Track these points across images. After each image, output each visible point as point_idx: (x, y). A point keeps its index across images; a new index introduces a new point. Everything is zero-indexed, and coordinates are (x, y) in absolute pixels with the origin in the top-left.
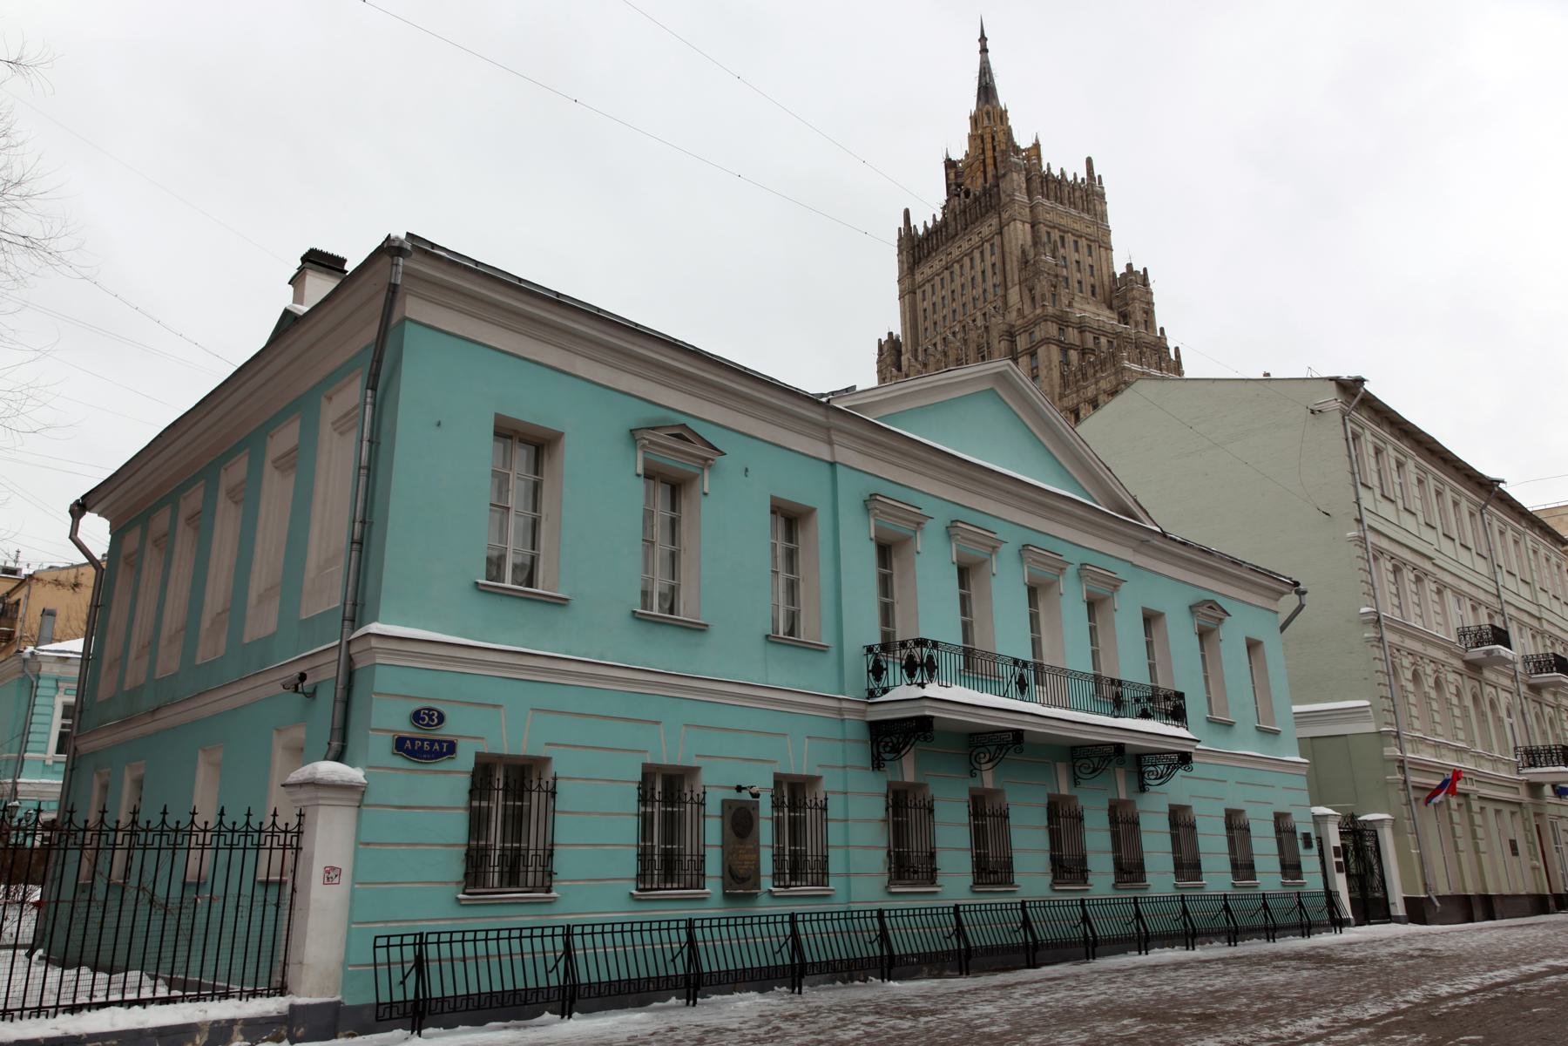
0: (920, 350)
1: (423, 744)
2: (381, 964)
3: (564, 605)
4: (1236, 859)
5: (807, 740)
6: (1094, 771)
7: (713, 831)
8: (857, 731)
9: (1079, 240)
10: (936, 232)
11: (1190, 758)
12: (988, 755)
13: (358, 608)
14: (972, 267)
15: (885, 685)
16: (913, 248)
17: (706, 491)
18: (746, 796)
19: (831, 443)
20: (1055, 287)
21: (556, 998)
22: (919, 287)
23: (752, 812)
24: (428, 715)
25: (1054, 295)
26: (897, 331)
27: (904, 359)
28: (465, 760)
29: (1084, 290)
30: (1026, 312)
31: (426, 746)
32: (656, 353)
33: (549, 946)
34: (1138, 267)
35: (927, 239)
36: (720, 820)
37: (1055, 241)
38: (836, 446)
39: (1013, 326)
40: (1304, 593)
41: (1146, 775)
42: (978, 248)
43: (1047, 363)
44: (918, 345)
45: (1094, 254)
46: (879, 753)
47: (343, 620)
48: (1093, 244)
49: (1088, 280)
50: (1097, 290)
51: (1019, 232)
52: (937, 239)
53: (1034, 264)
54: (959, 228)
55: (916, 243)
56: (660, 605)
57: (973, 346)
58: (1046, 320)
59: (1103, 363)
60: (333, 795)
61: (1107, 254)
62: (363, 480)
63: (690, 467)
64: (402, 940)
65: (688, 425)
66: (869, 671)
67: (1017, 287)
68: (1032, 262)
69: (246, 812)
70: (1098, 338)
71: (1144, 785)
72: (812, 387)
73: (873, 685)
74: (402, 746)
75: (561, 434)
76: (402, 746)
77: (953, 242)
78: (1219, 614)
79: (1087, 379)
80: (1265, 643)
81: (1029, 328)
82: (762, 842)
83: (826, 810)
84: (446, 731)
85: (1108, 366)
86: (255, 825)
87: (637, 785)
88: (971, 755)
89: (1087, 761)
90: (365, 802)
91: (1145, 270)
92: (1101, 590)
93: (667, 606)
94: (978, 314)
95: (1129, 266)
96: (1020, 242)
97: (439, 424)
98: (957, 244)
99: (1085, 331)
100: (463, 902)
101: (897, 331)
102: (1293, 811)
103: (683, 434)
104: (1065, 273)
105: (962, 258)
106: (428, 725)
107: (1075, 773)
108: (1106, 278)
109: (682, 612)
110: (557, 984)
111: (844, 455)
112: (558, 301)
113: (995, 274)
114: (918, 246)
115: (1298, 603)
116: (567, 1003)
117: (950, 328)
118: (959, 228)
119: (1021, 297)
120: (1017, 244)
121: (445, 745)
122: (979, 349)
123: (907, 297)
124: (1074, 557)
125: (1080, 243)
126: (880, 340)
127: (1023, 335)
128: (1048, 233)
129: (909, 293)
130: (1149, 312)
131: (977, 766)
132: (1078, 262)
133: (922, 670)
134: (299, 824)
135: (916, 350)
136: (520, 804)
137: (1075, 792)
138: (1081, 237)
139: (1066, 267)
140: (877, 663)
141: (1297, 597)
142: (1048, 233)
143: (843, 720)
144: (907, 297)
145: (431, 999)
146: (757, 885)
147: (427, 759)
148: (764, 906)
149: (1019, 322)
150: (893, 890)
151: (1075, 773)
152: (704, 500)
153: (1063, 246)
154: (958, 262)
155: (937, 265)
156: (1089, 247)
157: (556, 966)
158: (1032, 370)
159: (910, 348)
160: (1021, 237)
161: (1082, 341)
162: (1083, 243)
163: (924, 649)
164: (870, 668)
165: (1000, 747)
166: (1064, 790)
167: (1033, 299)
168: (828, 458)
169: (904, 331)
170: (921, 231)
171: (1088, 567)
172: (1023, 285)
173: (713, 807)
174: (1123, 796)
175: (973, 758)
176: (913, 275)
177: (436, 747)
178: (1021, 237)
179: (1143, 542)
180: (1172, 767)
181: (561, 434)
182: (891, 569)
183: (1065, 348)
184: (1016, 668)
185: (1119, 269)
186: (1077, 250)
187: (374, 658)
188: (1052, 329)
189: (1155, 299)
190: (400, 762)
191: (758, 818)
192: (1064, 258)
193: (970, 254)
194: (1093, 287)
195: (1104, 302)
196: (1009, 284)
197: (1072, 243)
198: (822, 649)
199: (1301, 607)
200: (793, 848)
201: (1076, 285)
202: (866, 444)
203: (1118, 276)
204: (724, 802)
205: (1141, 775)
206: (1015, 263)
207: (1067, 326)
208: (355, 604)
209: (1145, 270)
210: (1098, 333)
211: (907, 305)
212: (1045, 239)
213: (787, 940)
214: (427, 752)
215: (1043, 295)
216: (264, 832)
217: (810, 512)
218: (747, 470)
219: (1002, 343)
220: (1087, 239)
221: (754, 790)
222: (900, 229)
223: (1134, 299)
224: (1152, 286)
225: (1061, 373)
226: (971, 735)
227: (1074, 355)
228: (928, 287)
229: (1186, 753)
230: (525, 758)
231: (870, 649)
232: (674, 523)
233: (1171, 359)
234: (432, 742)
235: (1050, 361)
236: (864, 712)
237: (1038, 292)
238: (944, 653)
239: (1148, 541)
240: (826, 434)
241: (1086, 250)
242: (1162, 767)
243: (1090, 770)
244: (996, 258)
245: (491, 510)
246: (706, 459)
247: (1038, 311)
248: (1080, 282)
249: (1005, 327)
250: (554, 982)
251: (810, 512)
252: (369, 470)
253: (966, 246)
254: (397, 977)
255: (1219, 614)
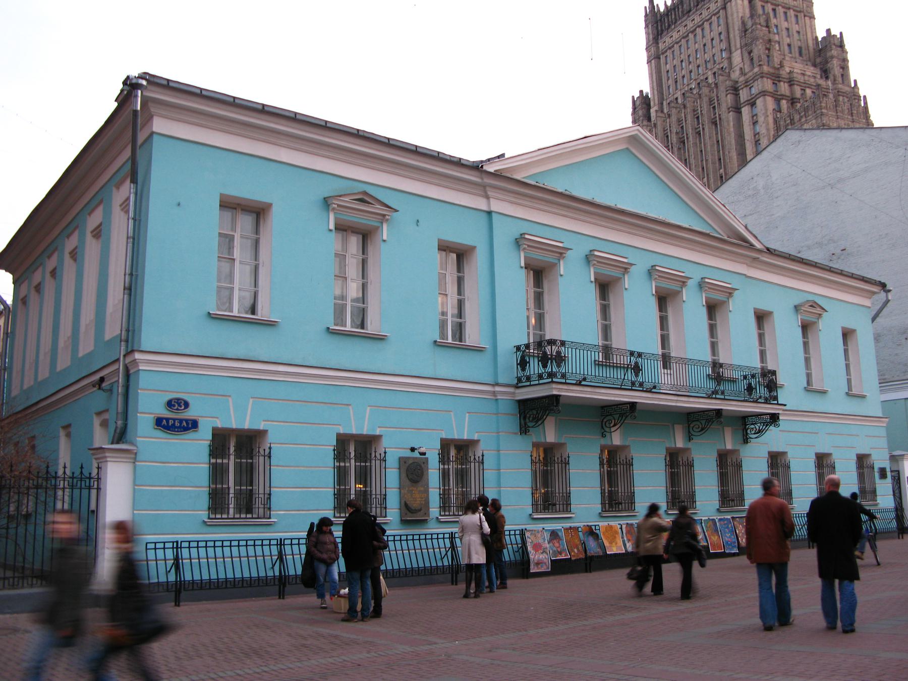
0: (665, 103)
1: (174, 422)
2: (194, 559)
3: (482, 351)
4: (865, 488)
5: (467, 414)
6: (702, 429)
7: (393, 477)
8: (507, 407)
9: (788, 11)
10: (674, 9)
11: (778, 418)
12: (613, 421)
13: (130, 333)
14: (703, 37)
15: (528, 374)
16: (657, 22)
17: (385, 237)
18: (416, 454)
19: (488, 198)
20: (769, 50)
21: (448, 572)
22: (663, 54)
23: (423, 466)
24: (177, 403)
25: (768, 56)
26: (647, 89)
27: (653, 111)
28: (204, 435)
29: (793, 51)
30: (747, 71)
31: (177, 424)
32: (345, 141)
33: (267, 552)
34: (835, 32)
35: (667, 15)
36: (398, 470)
37: (768, 13)
38: (491, 199)
39: (737, 82)
40: (890, 291)
41: (749, 431)
42: (707, 20)
43: (763, 112)
44: (663, 99)
45: (800, 22)
46: (525, 424)
47: (121, 342)
48: (799, 14)
49: (796, 44)
50: (804, 51)
51: (739, 7)
52: (675, 15)
53: (752, 32)
54: (692, 5)
55: (659, 18)
56: (352, 321)
57: (705, 100)
58: (762, 77)
59: (806, 110)
60: (122, 455)
61: (811, 22)
62: (130, 245)
63: (372, 222)
64: (231, 543)
65: (367, 191)
66: (517, 364)
67: (739, 51)
68: (750, 30)
69: (63, 466)
70: (804, 90)
71: (747, 439)
72: (472, 155)
73: (521, 374)
74: (160, 423)
75: (270, 205)
76: (160, 423)
77: (689, 16)
78: (818, 311)
79: (794, 123)
80: (858, 332)
81: (748, 84)
82: (431, 485)
83: (483, 463)
84: (190, 414)
85: (810, 113)
86: (86, 474)
87: (333, 448)
88: (602, 422)
89: (699, 423)
90: (138, 459)
91: (841, 34)
92: (717, 296)
93: (359, 323)
94: (710, 73)
95: (828, 31)
96: (740, 15)
97: (179, 205)
98: (691, 18)
99: (794, 84)
100: (208, 524)
101: (647, 89)
102: (872, 452)
103: (364, 199)
104: (777, 38)
105: (695, 30)
106: (177, 409)
107: (689, 432)
108: (810, 43)
109: (369, 328)
110: (448, 564)
111: (496, 206)
112: (264, 110)
113: (721, 41)
114: (661, 20)
115: (885, 299)
116: (454, 575)
117: (688, 85)
118: (692, 5)
119: (742, 59)
120: (738, 17)
121: (190, 422)
122: (711, 102)
123: (653, 61)
124: (695, 275)
125: (788, 14)
126: (633, 97)
127: (744, 89)
128: (763, 7)
129: (654, 58)
130: (844, 66)
131: (607, 430)
132: (788, 29)
133: (552, 362)
134: (98, 473)
135: (662, 104)
136: (251, 461)
137: (689, 445)
138: (789, 9)
139: (778, 33)
140: (523, 358)
141: (885, 294)
142: (763, 7)
143: (497, 400)
144: (653, 61)
145: (289, 575)
146: (427, 513)
147: (178, 431)
148: (433, 528)
149: (741, 79)
150: (535, 517)
151: (689, 432)
152: (383, 245)
153: (775, 16)
154: (692, 32)
155: (675, 36)
156: (796, 16)
157: (446, 554)
158: (753, 117)
159: (657, 102)
160: (741, 10)
161: (792, 92)
162: (791, 13)
163: (553, 347)
164: (518, 362)
165: (621, 415)
166: (680, 444)
167: (752, 59)
168: (485, 208)
169: (652, 88)
170: (662, 9)
171: (707, 280)
172: (744, 49)
173: (392, 462)
174: (729, 446)
175: (604, 423)
176: (658, 43)
177: (184, 424)
178: (741, 10)
179: (755, 259)
180: (767, 424)
181: (270, 205)
182: (542, 288)
183: (778, 99)
184: (632, 358)
185: (821, 34)
186: (786, 20)
187: (138, 366)
188: (768, 85)
189: (849, 57)
190: (159, 433)
191: (428, 469)
192: (777, 26)
193: (701, 26)
194: (800, 48)
195: (810, 60)
196: (733, 49)
197: (782, 14)
198: (479, 350)
199: (888, 301)
200: (609, 469)
201: (786, 47)
202: (516, 196)
203: (820, 39)
204: (400, 459)
205: (745, 430)
206: (737, 32)
207: (779, 81)
208: (128, 331)
209: (841, 34)
210: (804, 86)
211: (653, 67)
212: (760, 11)
213: (447, 552)
214: (177, 427)
215: (759, 57)
216: (92, 478)
217: (472, 249)
218: (418, 221)
219: (729, 96)
220: (794, 10)
221: (422, 450)
222: (646, 7)
223: (832, 57)
224: (846, 47)
225: (774, 119)
226: (603, 407)
227: (784, 104)
228: (669, 53)
229: (775, 414)
230: (249, 430)
231: (518, 348)
232: (364, 262)
233: (860, 105)
234: (181, 421)
235: (766, 110)
236: (514, 393)
237: (755, 54)
238: (570, 350)
239: (758, 258)
240: (483, 191)
241: (793, 19)
242: (759, 424)
243: (700, 429)
244: (722, 28)
245: (218, 260)
246: (384, 216)
247: (756, 70)
248: (789, 45)
249: (728, 83)
250: (446, 563)
251: (472, 249)
252: (134, 239)
253: (697, 19)
254: (269, 565)
255: (818, 311)
